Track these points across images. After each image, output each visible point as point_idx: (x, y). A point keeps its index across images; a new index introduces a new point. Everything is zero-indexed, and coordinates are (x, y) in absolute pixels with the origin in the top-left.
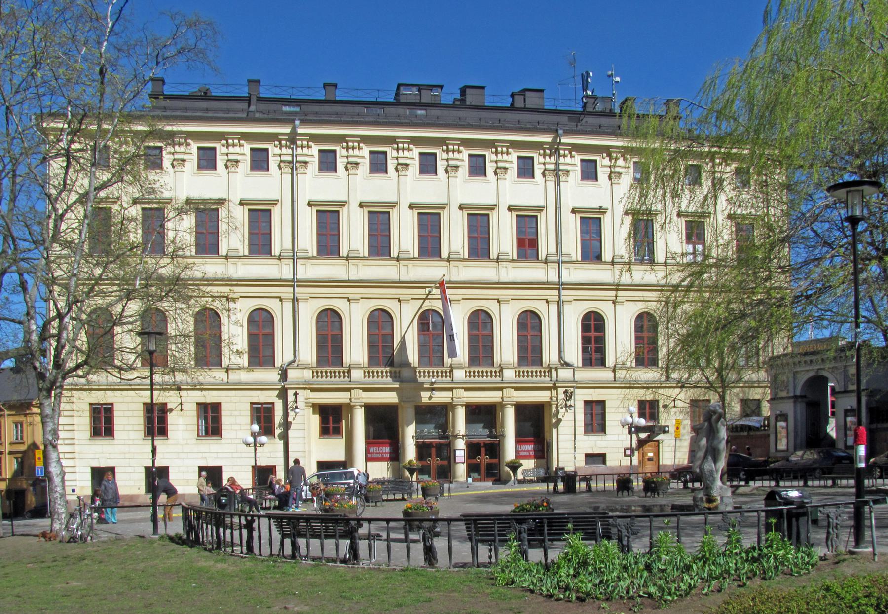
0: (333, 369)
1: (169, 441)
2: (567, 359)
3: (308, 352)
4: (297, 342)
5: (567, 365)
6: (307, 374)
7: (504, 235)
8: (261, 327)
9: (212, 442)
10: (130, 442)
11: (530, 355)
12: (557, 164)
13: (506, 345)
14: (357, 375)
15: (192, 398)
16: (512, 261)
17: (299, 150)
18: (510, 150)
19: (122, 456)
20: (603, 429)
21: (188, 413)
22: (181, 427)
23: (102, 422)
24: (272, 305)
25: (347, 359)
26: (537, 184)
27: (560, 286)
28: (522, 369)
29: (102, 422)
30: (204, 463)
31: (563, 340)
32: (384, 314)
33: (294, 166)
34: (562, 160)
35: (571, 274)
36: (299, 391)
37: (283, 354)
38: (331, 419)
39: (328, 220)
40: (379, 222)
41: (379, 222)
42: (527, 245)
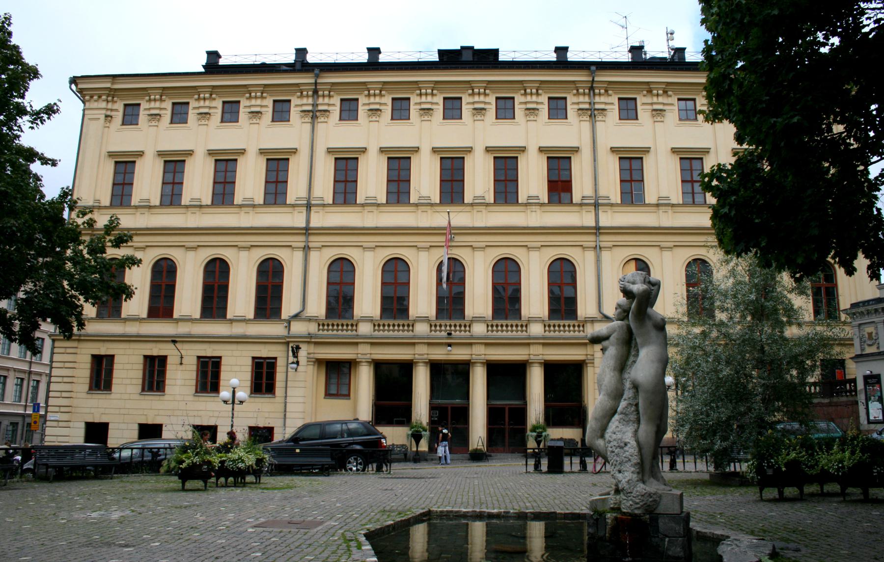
0: (567, 322)
1: (166, 397)
3: (317, 306)
4: (305, 291)
6: (313, 328)
7: (533, 178)
8: (270, 278)
9: (201, 399)
10: (126, 396)
12: (315, 105)
13: (535, 298)
14: (365, 329)
15: (191, 353)
17: (597, 99)
18: (435, 92)
19: (117, 412)
20: (108, 387)
21: (188, 368)
22: (179, 382)
23: (101, 374)
24: (282, 255)
25: (525, 312)
26: (517, 124)
27: (598, 230)
28: (552, 322)
29: (101, 374)
32: (509, 261)
33: (593, 113)
34: (320, 100)
36: (301, 345)
37: (290, 305)
38: (337, 374)
39: (346, 166)
40: (506, 167)
41: (506, 167)
42: (560, 187)
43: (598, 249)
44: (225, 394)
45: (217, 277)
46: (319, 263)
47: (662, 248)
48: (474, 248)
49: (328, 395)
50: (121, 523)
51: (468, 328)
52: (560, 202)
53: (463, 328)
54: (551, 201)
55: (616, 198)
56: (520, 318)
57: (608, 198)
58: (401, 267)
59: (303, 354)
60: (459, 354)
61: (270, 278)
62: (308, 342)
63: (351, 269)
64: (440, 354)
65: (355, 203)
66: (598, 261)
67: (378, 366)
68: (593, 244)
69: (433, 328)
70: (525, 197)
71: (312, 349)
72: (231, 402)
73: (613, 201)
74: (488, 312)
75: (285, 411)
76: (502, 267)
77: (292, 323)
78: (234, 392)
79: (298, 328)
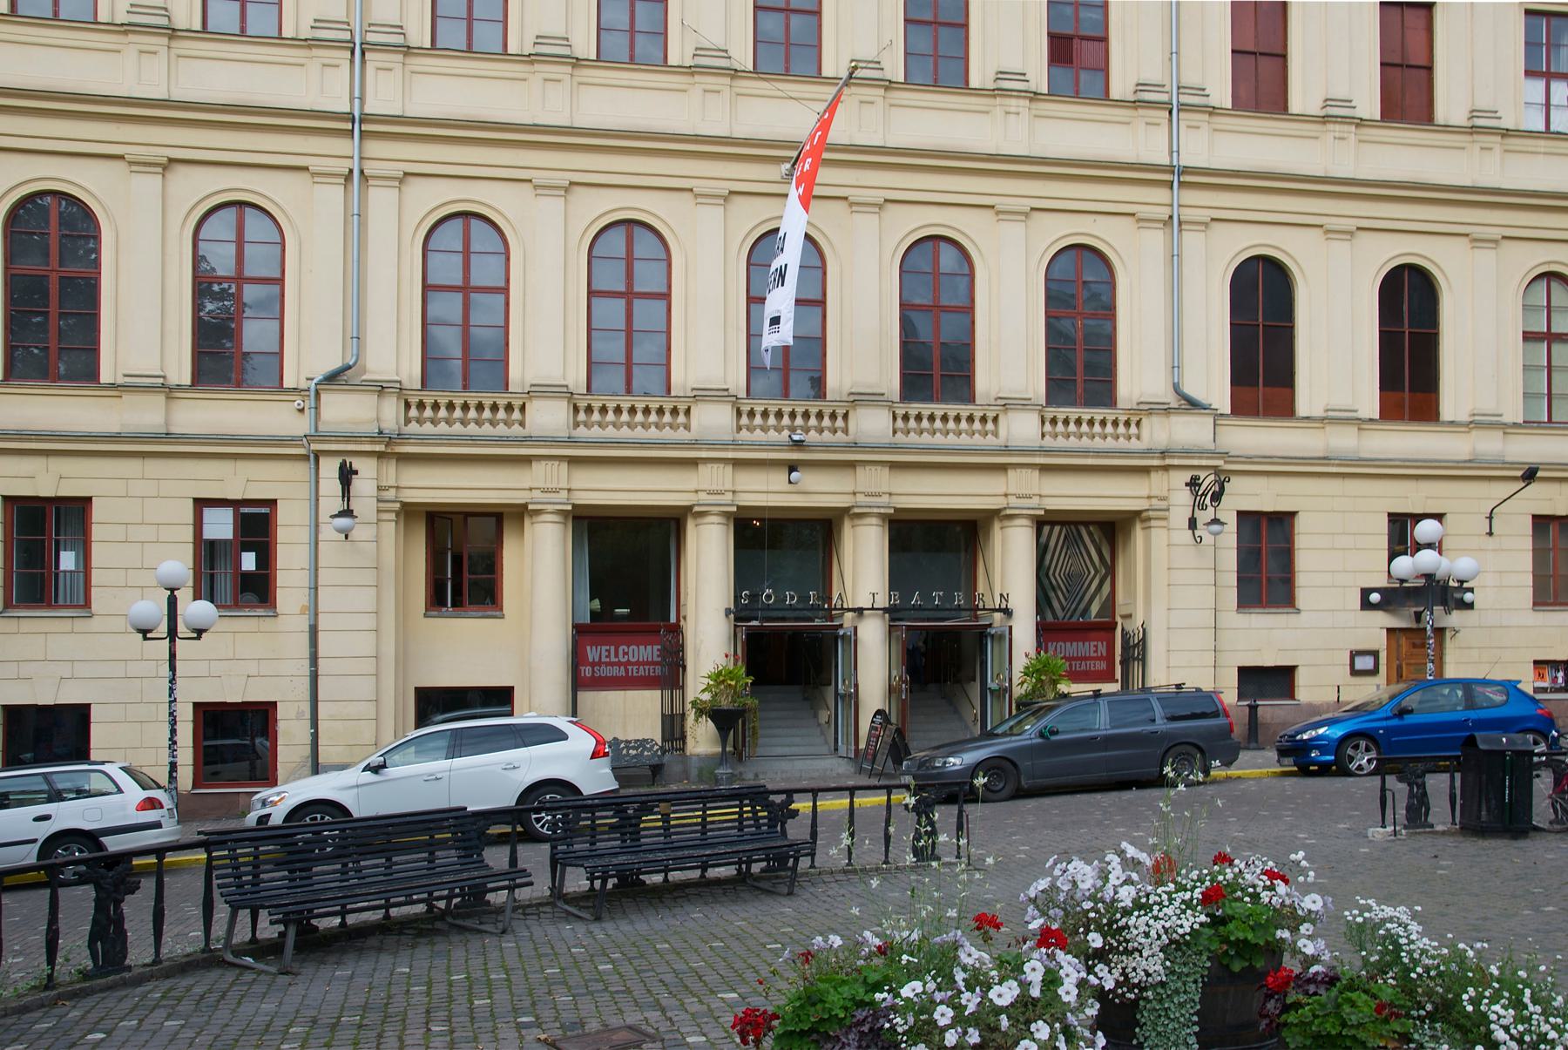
2: (1190, 390)
3: (395, 354)
4: (349, 302)
5: (1193, 405)
6: (390, 414)
9: (26, 625)
11: (1079, 378)
16: (1035, 96)
28: (914, 408)
30: (1469, 612)
31: (1172, 336)
32: (1087, 254)
35: (1202, 146)
36: (357, 463)
43: (356, 179)
44: (196, 610)
45: (1263, 307)
46: (398, 221)
47: (1477, 241)
48: (852, 204)
49: (437, 600)
50: (884, 953)
51: (840, 423)
52: (1077, 94)
53: (826, 422)
54: (1054, 93)
55: (1221, 92)
56: (971, 399)
57: (1201, 91)
58: (948, 258)
59: (364, 485)
60: (818, 491)
61: (1409, 304)
62: (380, 456)
63: (1105, 276)
64: (767, 491)
65: (962, 84)
66: (1174, 258)
67: (1043, 523)
68: (1164, 213)
69: (413, 412)
70: (530, 39)
71: (390, 472)
72: (163, 629)
73: (1214, 101)
74: (1034, 382)
75: (314, 659)
76: (922, 262)
77: (324, 396)
78: (172, 603)
79: (346, 412)
